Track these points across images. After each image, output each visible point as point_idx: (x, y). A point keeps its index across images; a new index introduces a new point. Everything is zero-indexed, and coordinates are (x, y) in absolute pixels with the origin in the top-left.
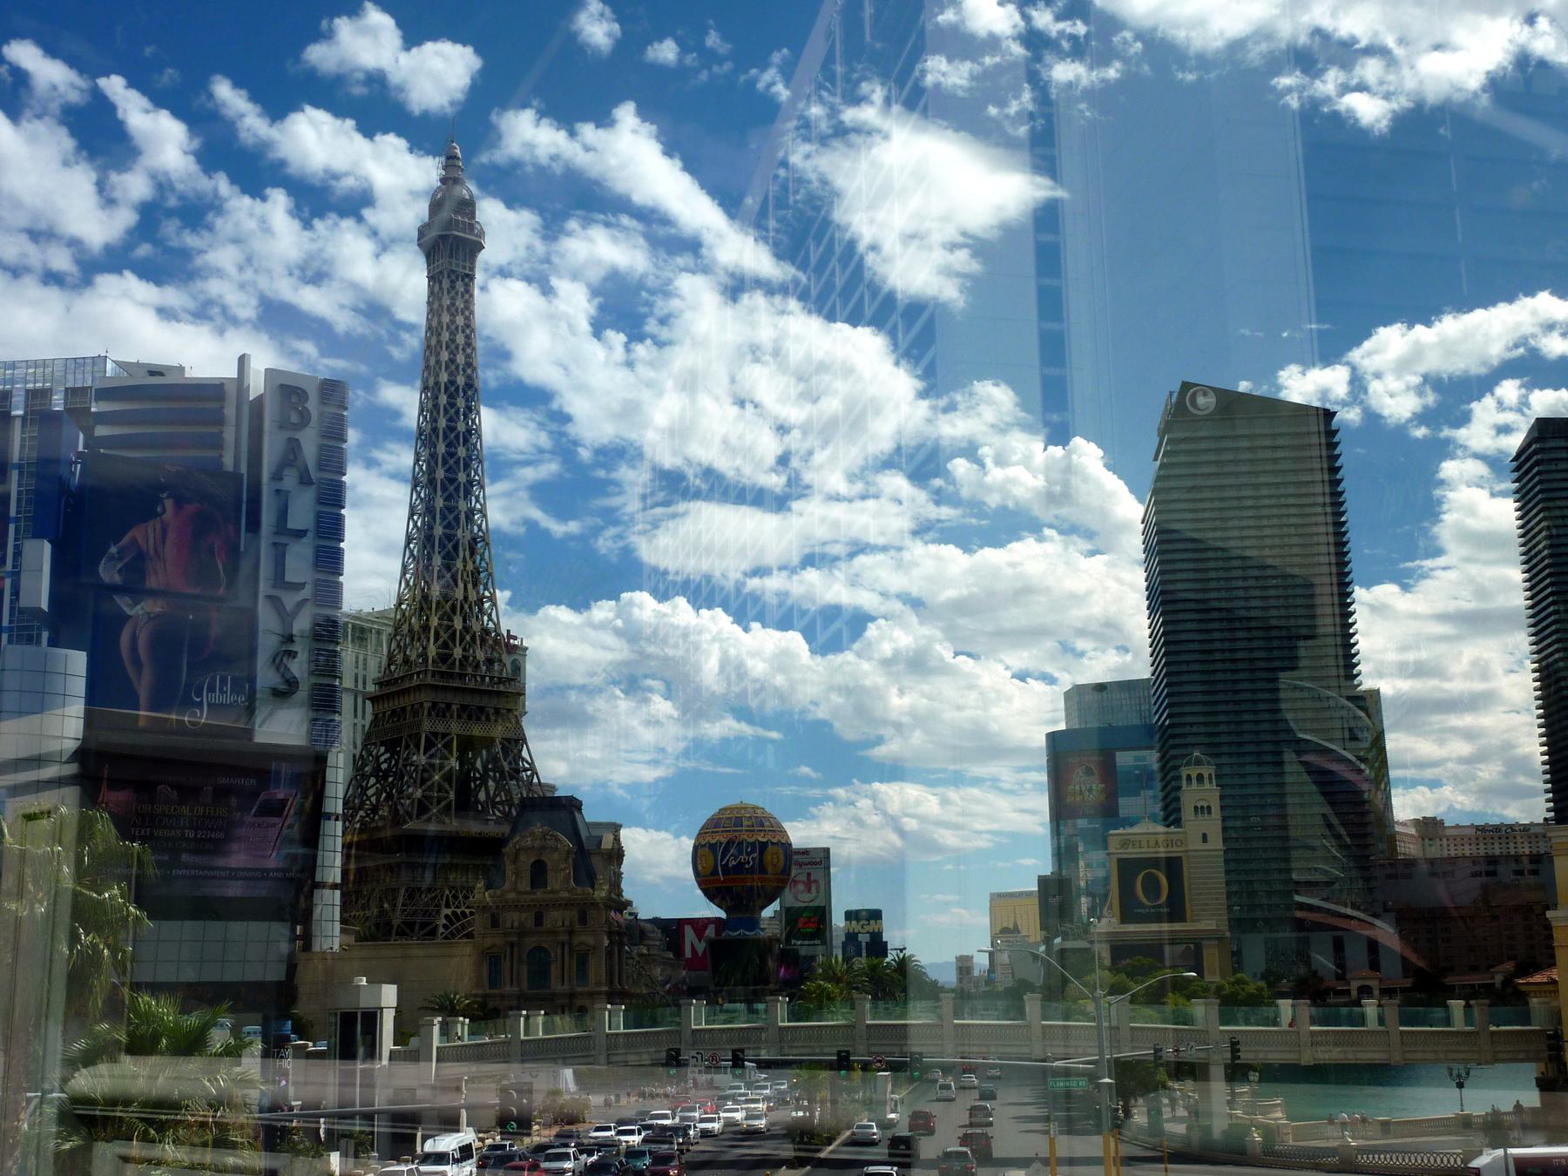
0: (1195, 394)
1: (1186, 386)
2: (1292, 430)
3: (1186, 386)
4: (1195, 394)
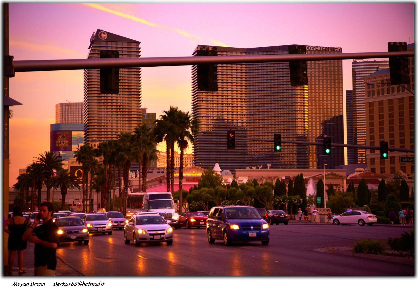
0: (101, 33)
1: (99, 31)
2: (128, 47)
3: (99, 31)
4: (101, 33)
